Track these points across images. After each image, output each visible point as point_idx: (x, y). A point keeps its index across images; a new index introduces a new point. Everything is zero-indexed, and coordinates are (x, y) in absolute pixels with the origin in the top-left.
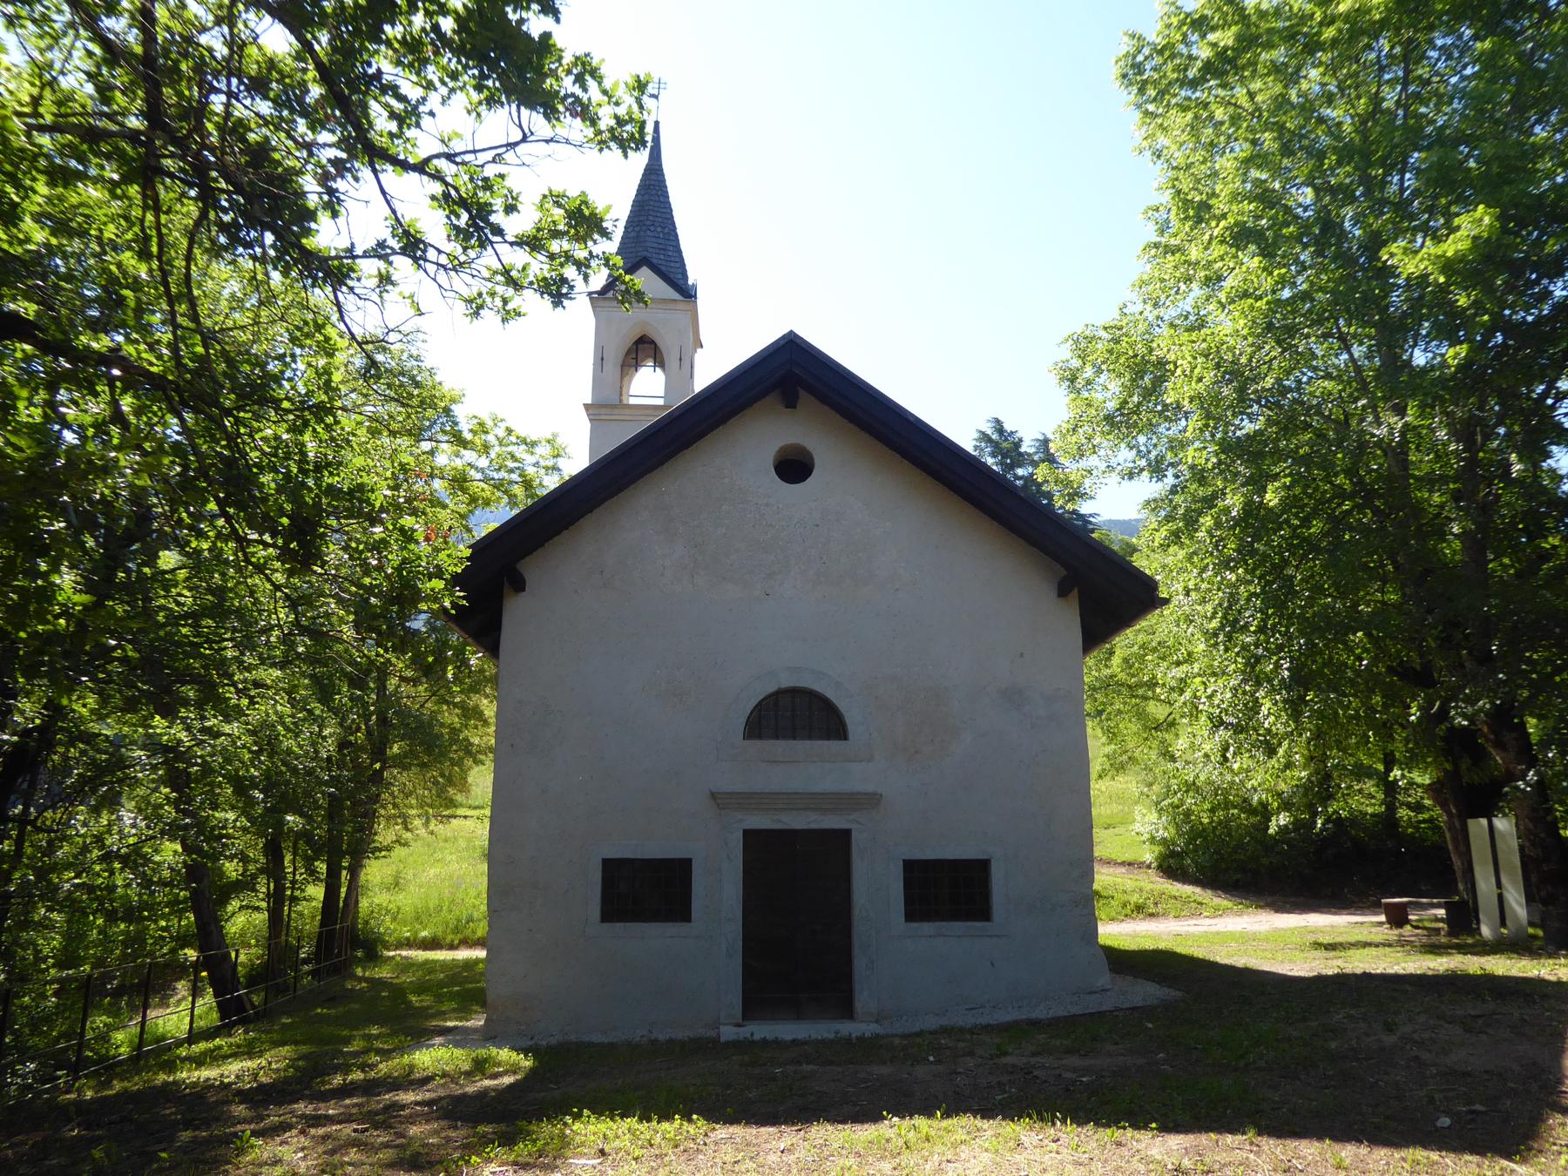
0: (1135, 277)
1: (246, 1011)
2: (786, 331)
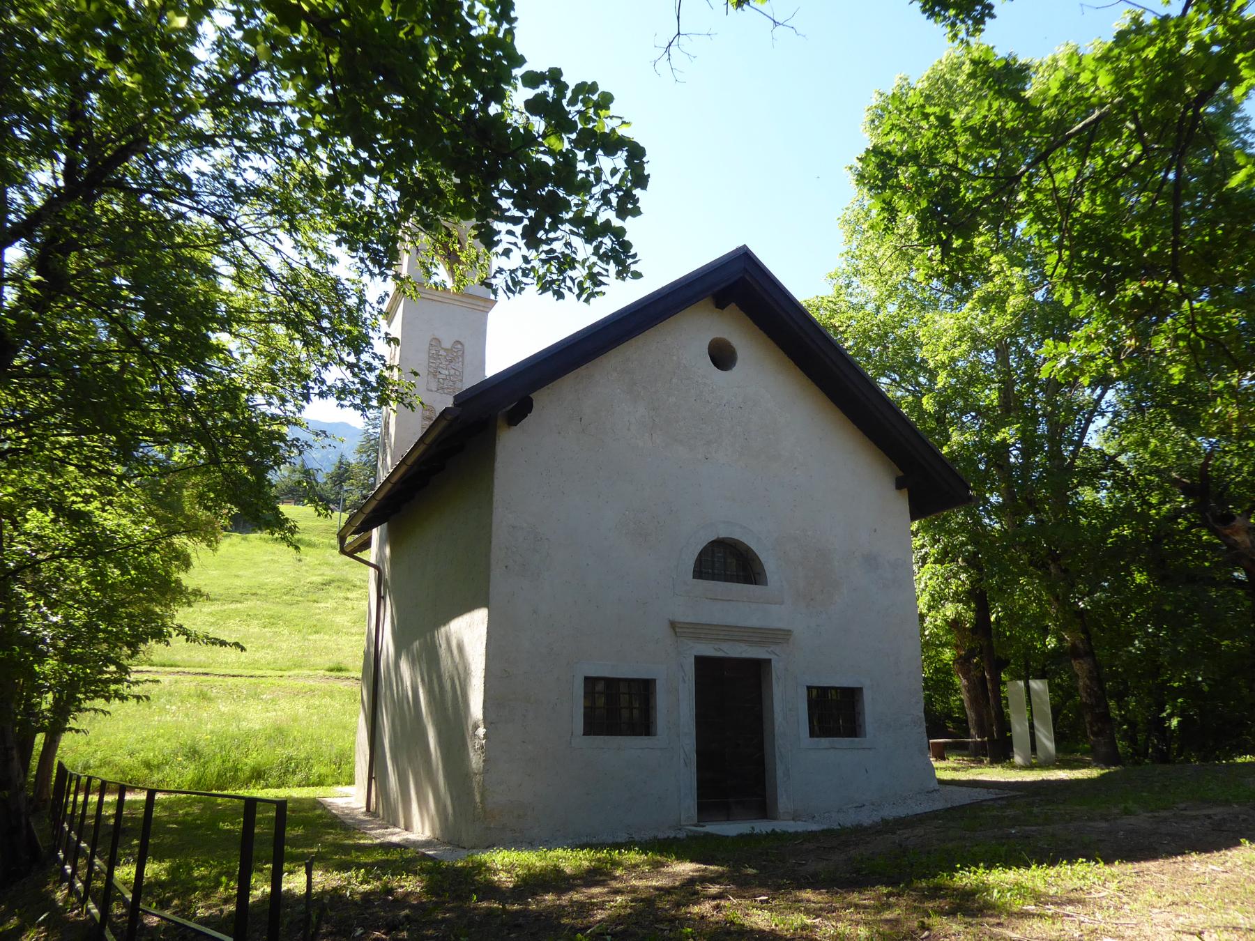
0: (833, 270)
1: (969, 736)
2: (741, 244)
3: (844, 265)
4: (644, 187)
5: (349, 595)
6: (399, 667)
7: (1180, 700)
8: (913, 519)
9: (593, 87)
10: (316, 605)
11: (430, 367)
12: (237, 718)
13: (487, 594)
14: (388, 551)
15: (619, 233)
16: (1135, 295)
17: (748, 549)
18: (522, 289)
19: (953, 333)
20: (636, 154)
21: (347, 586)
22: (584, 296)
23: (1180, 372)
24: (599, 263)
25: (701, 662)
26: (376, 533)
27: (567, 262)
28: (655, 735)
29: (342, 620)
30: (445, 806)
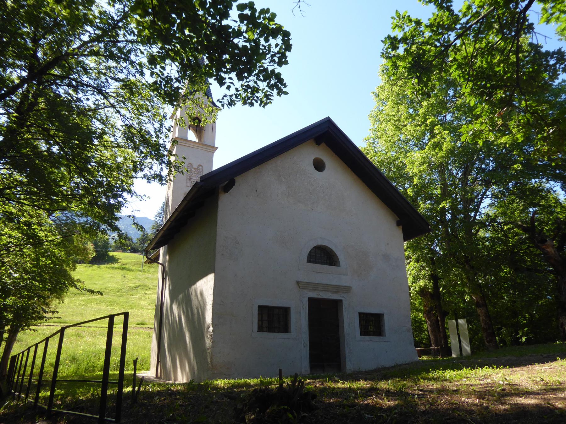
3: (371, 134)
4: (290, 51)
5: (147, 292)
6: (172, 308)
7: (526, 329)
8: (405, 241)
9: (267, 11)
10: (131, 296)
11: (187, 176)
12: (95, 344)
13: (214, 266)
14: (167, 257)
15: (278, 76)
16: (501, 97)
17: (331, 251)
18: (235, 104)
19: (420, 160)
20: (286, 35)
21: (146, 288)
22: (262, 105)
23: (522, 137)
24: (269, 90)
25: (311, 300)
26: (162, 250)
27: (255, 90)
28: (290, 333)
29: (144, 303)
30: (193, 367)
